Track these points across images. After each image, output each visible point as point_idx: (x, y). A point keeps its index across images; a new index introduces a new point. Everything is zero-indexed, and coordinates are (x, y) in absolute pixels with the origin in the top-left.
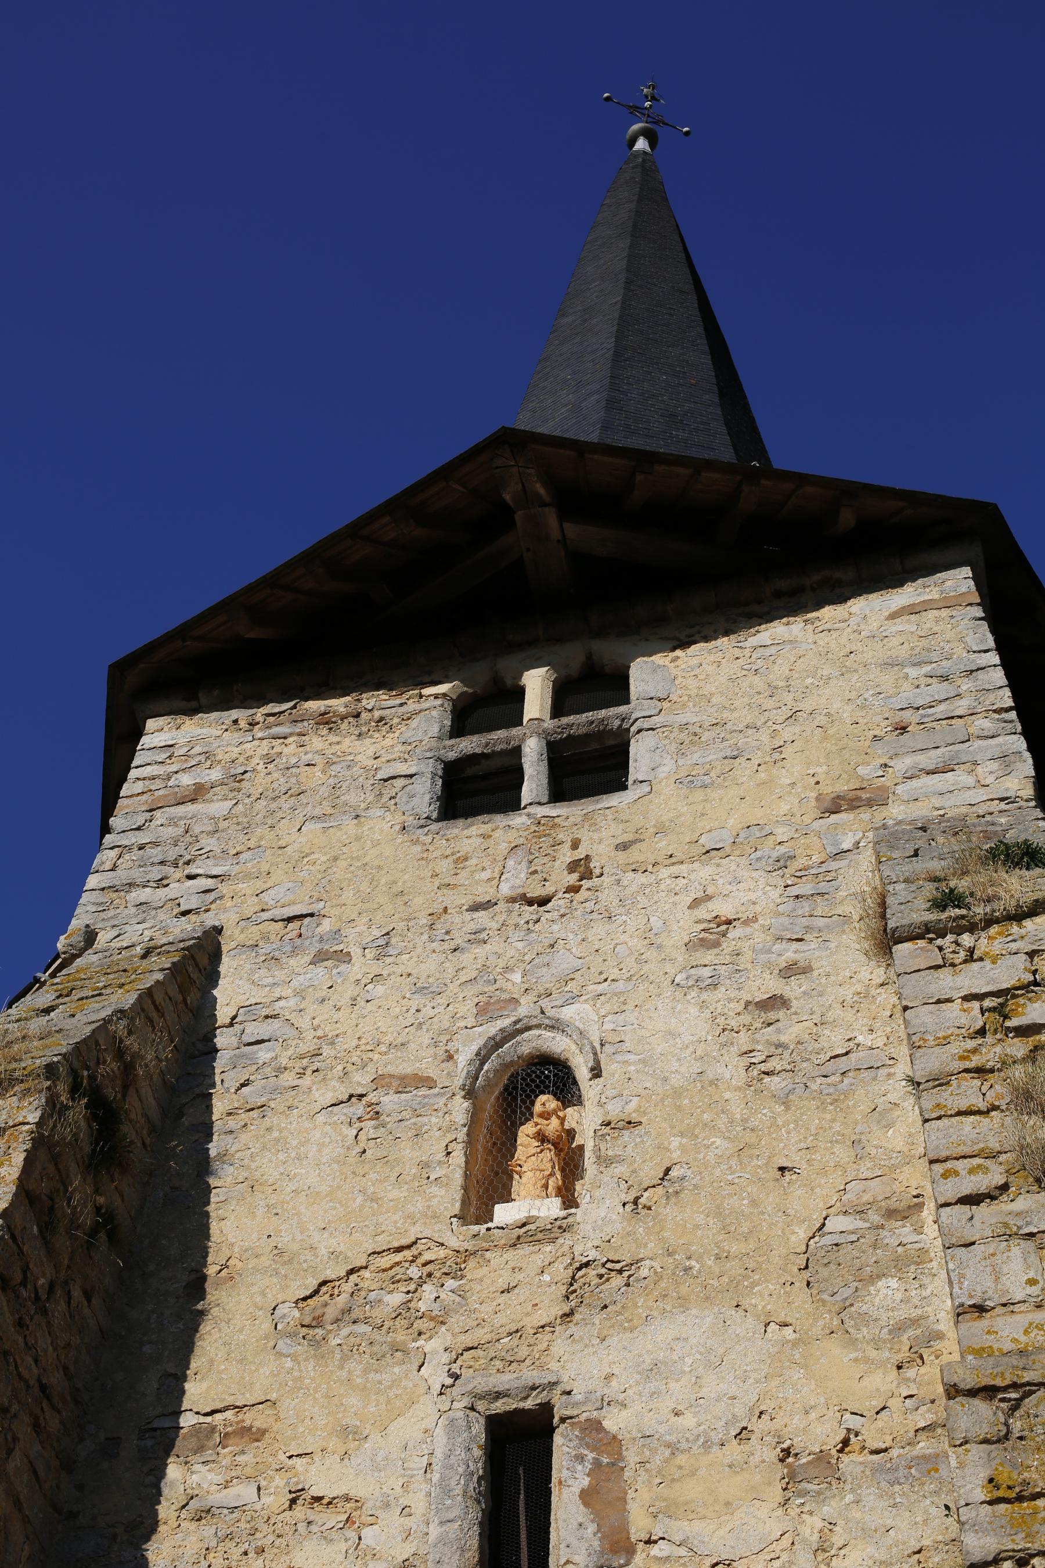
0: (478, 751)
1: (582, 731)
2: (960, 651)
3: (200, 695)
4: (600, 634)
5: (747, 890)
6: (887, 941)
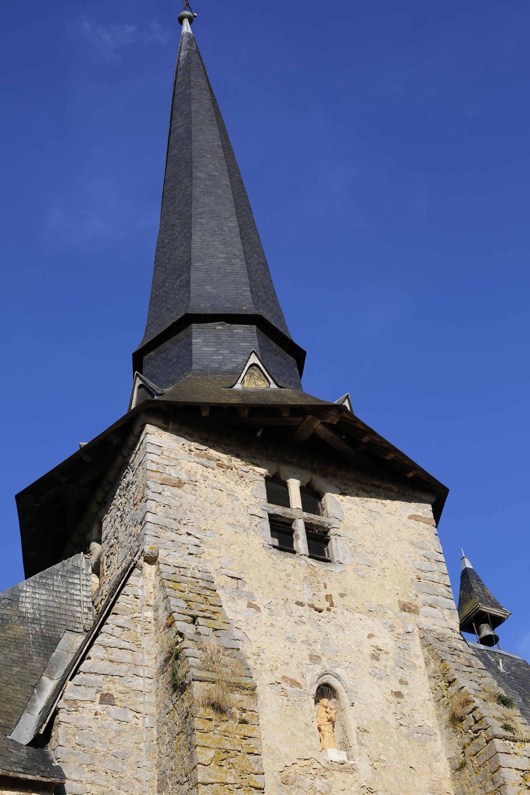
0: (281, 514)
1: (316, 523)
2: (432, 549)
3: (170, 424)
4: (324, 475)
5: (385, 640)
6: (429, 677)
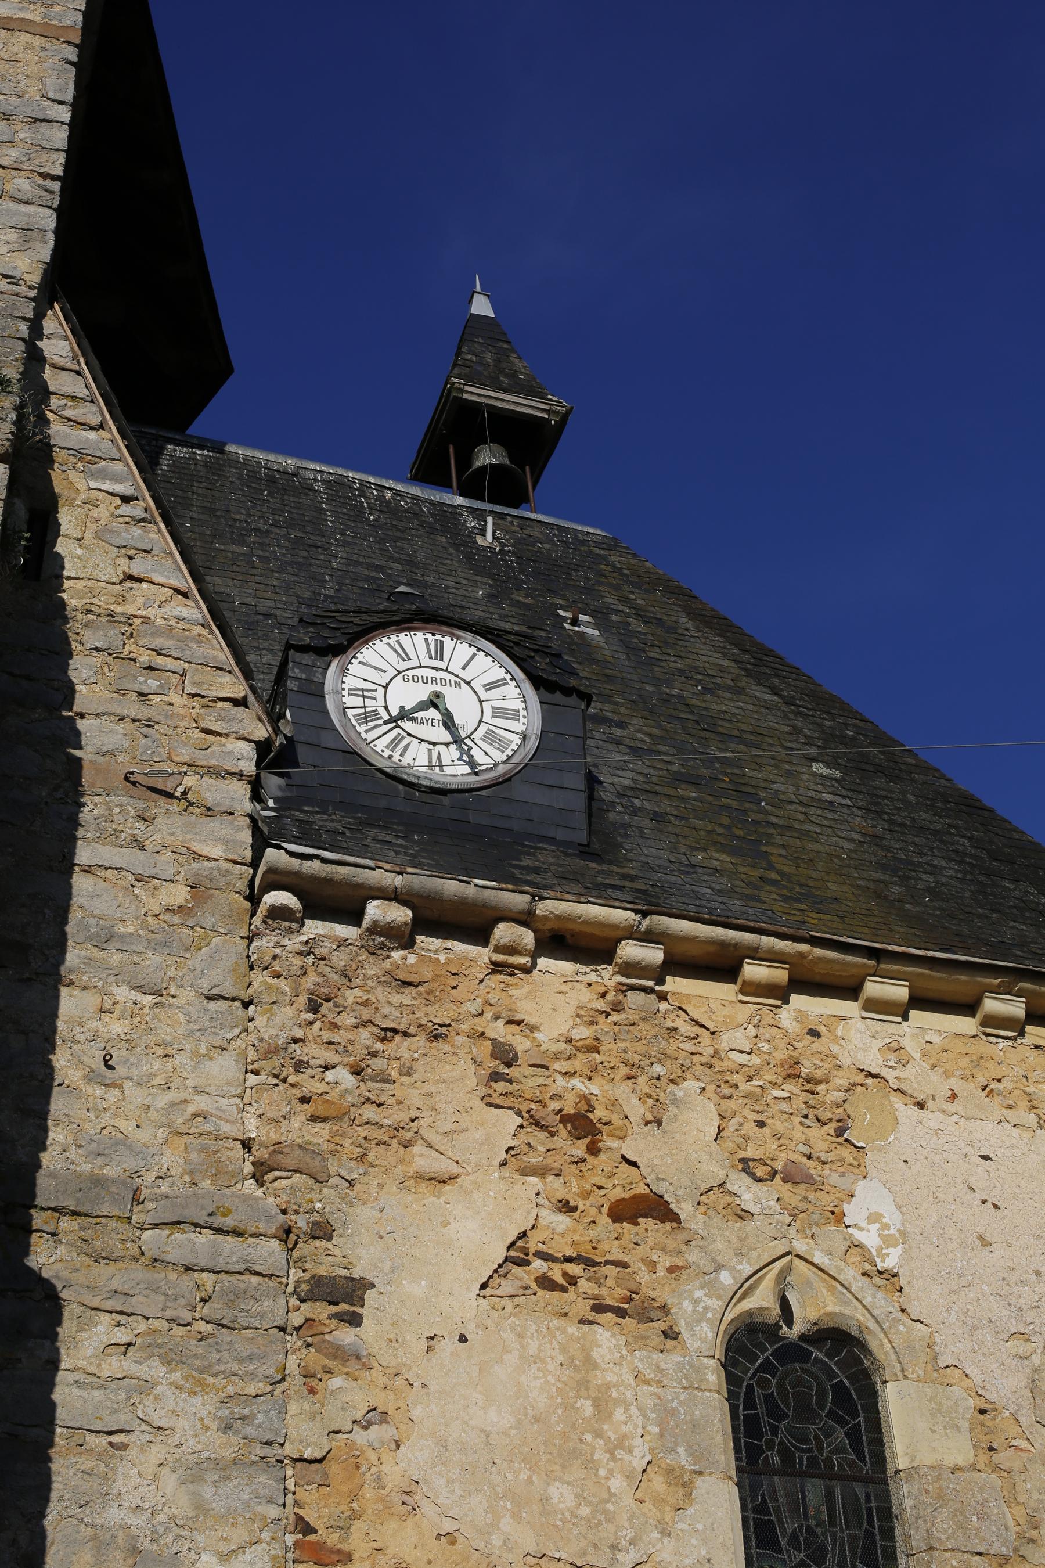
2: (33, 92)
